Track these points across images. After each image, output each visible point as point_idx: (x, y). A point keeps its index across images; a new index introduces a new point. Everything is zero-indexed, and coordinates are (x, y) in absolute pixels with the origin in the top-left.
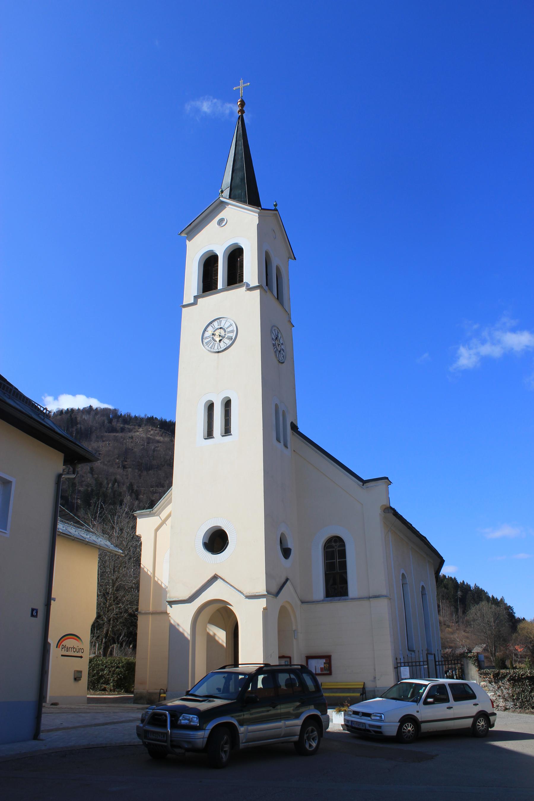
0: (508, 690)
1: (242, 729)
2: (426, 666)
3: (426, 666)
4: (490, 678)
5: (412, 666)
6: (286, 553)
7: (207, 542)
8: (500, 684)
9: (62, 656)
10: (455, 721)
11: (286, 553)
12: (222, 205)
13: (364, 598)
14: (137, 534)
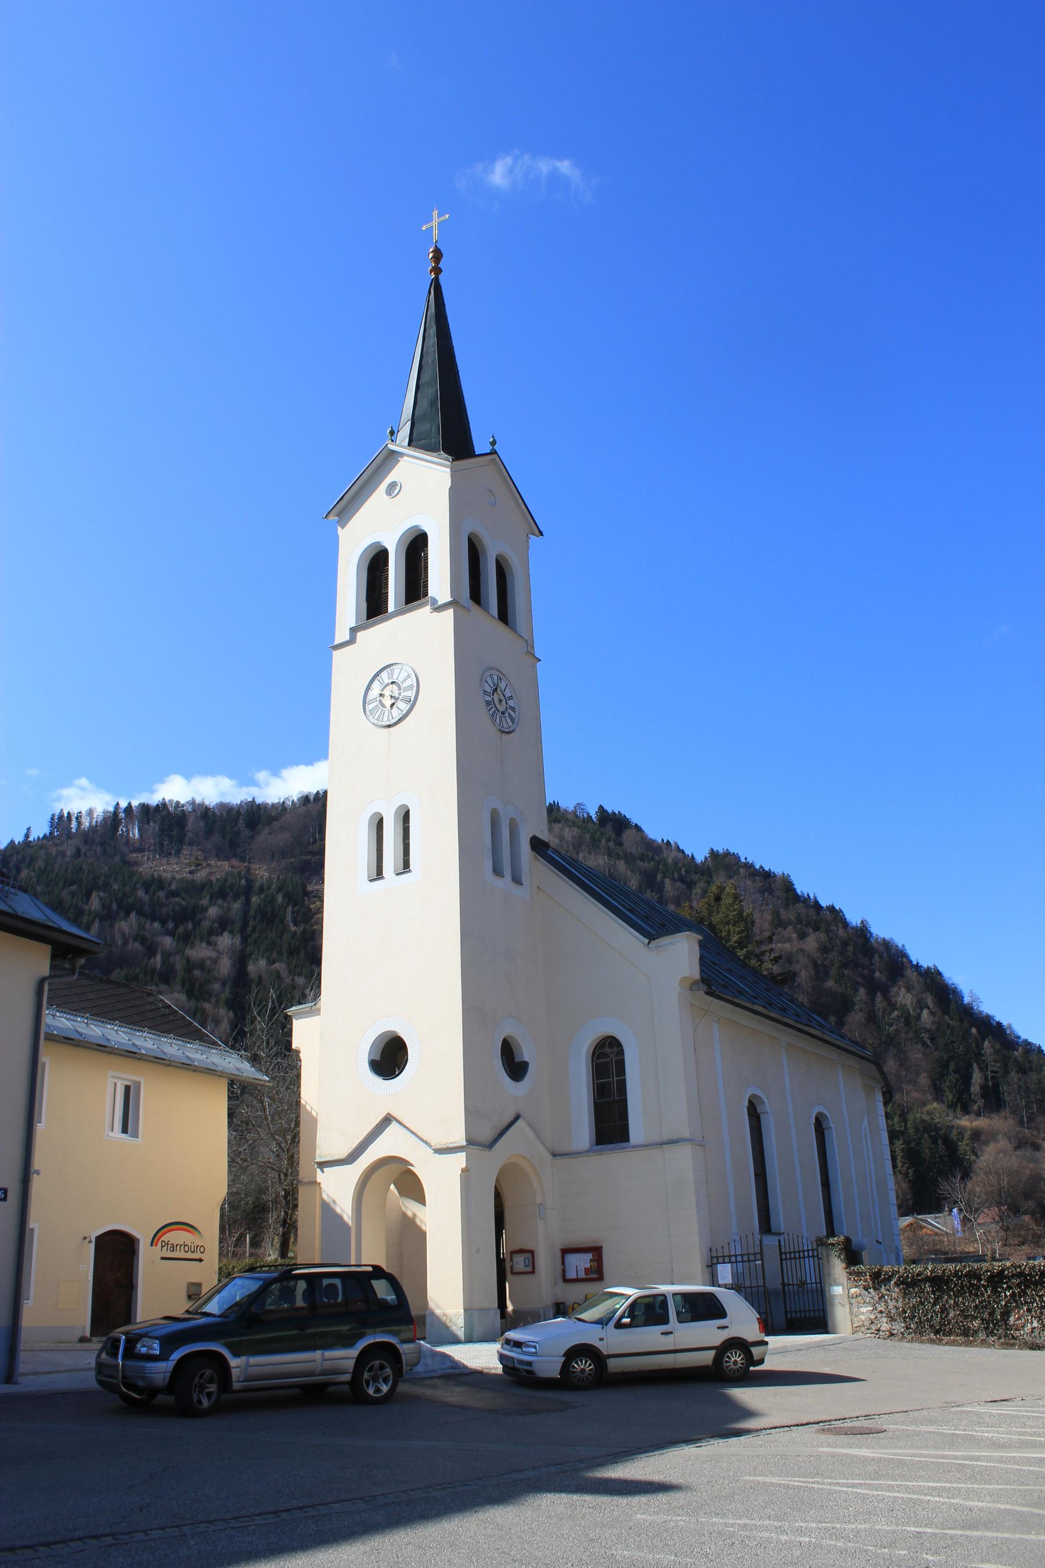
0: (897, 1301)
1: (234, 1362)
2: (759, 1262)
3: (759, 1262)
4: (866, 1281)
5: (737, 1262)
6: (516, 1069)
7: (378, 1058)
8: (883, 1290)
9: (162, 1258)
10: (677, 1355)
11: (516, 1069)
12: (391, 458)
13: (654, 1144)
14: (294, 1047)
